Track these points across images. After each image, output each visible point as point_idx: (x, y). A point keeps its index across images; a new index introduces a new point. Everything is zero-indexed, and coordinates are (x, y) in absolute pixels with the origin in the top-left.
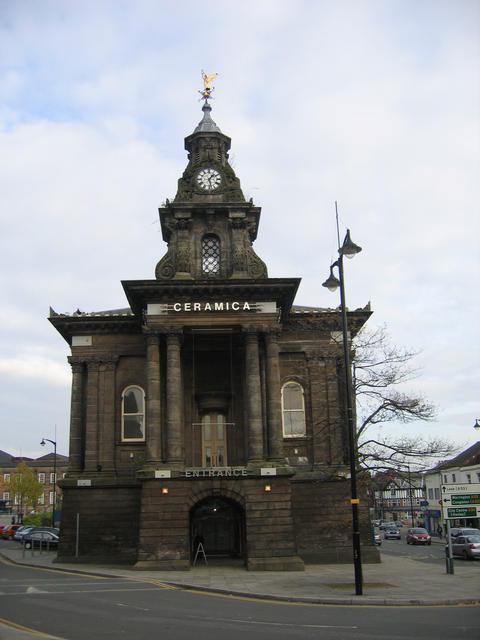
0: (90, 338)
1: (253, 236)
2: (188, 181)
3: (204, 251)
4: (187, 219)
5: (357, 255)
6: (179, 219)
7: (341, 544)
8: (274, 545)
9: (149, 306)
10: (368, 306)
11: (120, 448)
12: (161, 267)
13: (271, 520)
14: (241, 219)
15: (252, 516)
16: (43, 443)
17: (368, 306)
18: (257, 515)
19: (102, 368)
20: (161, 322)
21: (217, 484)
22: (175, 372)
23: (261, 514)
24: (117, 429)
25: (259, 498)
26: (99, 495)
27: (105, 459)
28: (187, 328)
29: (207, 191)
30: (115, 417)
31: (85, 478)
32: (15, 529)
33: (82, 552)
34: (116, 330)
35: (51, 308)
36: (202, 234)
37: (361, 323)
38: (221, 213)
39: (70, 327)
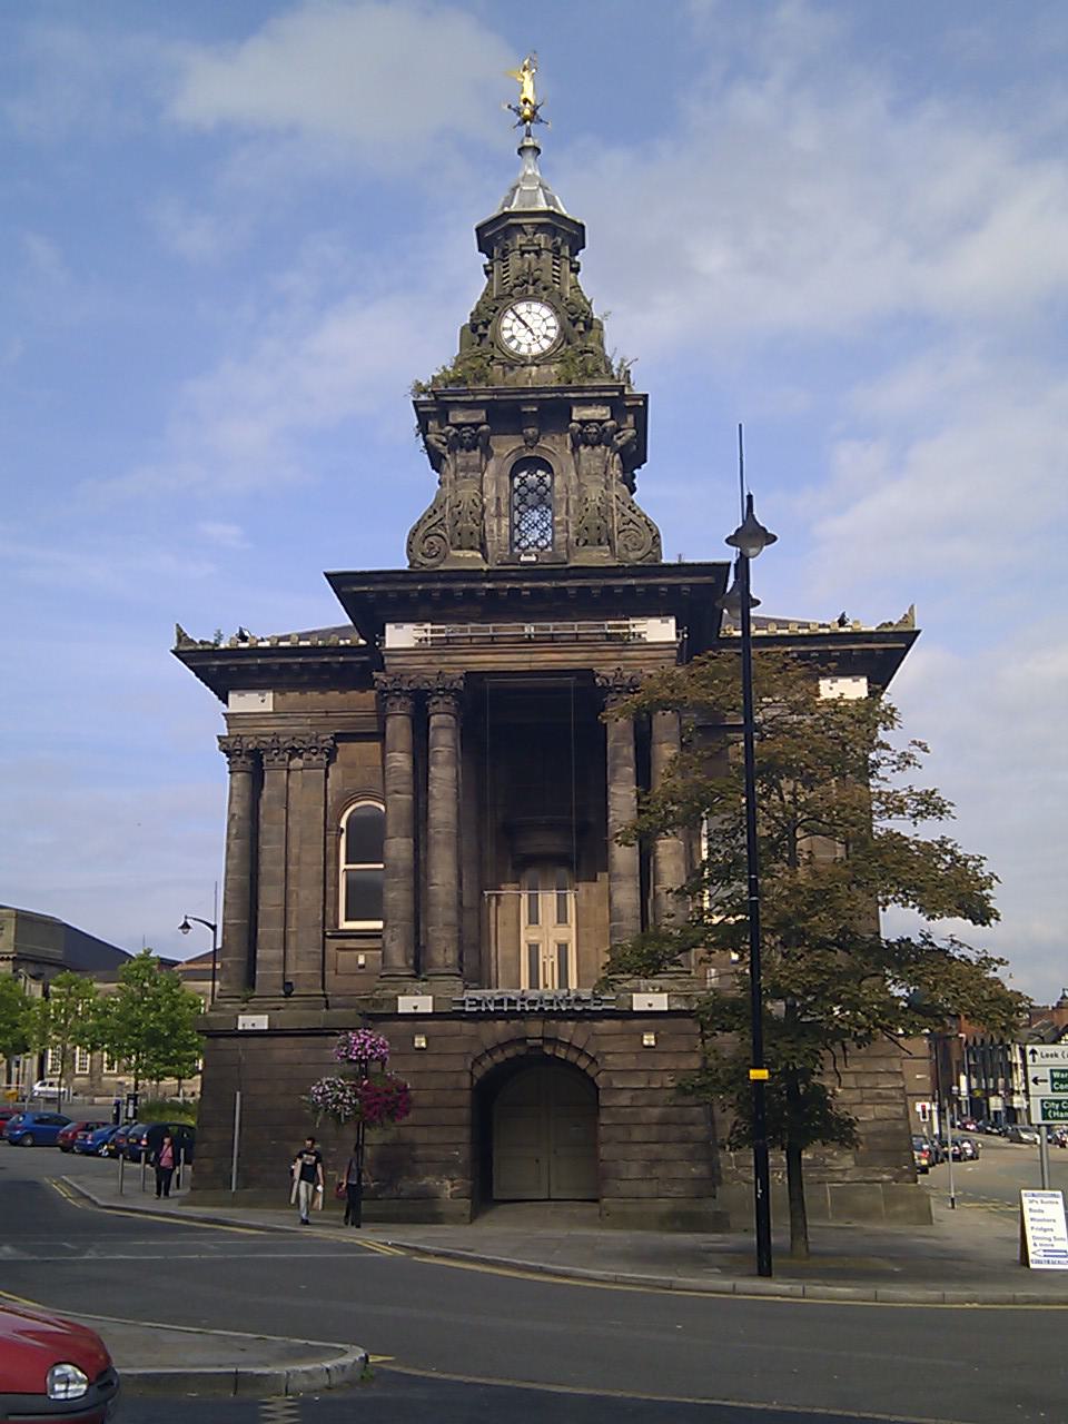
0: (269, 695)
1: (634, 456)
2: (481, 328)
3: (516, 498)
4: (476, 425)
6: (458, 426)
7: (838, 1176)
8: (659, 1171)
9: (389, 628)
10: (906, 619)
11: (333, 944)
12: (634, 476)
14: (601, 422)
15: (614, 1101)
16: (186, 926)
18: (624, 1099)
19: (297, 762)
20: (418, 663)
21: (535, 1028)
22: (443, 776)
24: (328, 900)
25: (629, 1062)
26: (284, 1049)
27: (302, 969)
28: (471, 677)
29: (522, 357)
31: (256, 1012)
33: (246, 1180)
36: (512, 459)
38: (552, 411)
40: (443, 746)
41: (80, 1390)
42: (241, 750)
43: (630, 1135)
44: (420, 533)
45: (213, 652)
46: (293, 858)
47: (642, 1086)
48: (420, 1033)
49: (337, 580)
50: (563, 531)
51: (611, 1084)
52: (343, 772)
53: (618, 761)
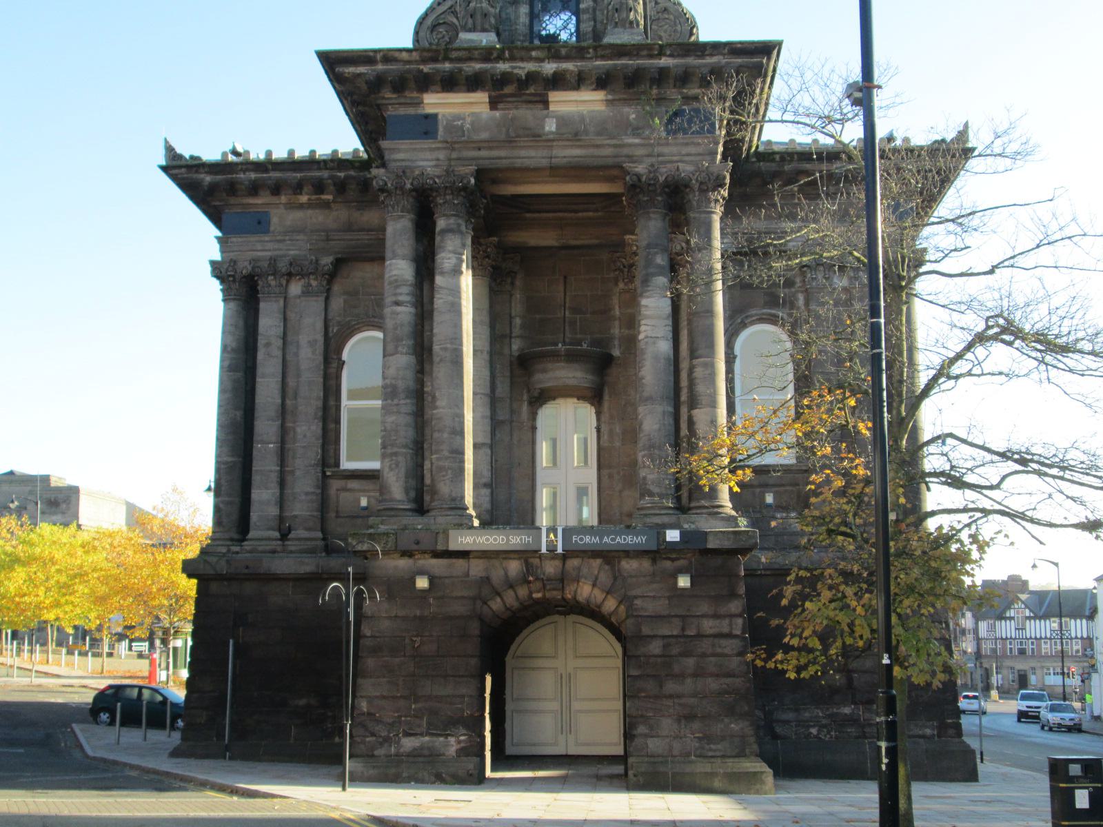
5: (785, 62)
10: (963, 135)
13: (690, 662)
17: (963, 135)
19: (295, 288)
23: (665, 646)
30: (325, 408)
32: (1014, 340)
33: (240, 732)
34: (508, 90)
35: (166, 142)
37: (945, 179)
39: (213, 188)
40: (450, 252)
41: (903, 271)
42: (233, 276)
43: (661, 687)
44: (429, 21)
45: (196, 165)
46: (290, 392)
47: (675, 633)
48: (422, 573)
49: (332, 62)
50: (589, 20)
51: (640, 630)
52: (345, 301)
53: (651, 270)
